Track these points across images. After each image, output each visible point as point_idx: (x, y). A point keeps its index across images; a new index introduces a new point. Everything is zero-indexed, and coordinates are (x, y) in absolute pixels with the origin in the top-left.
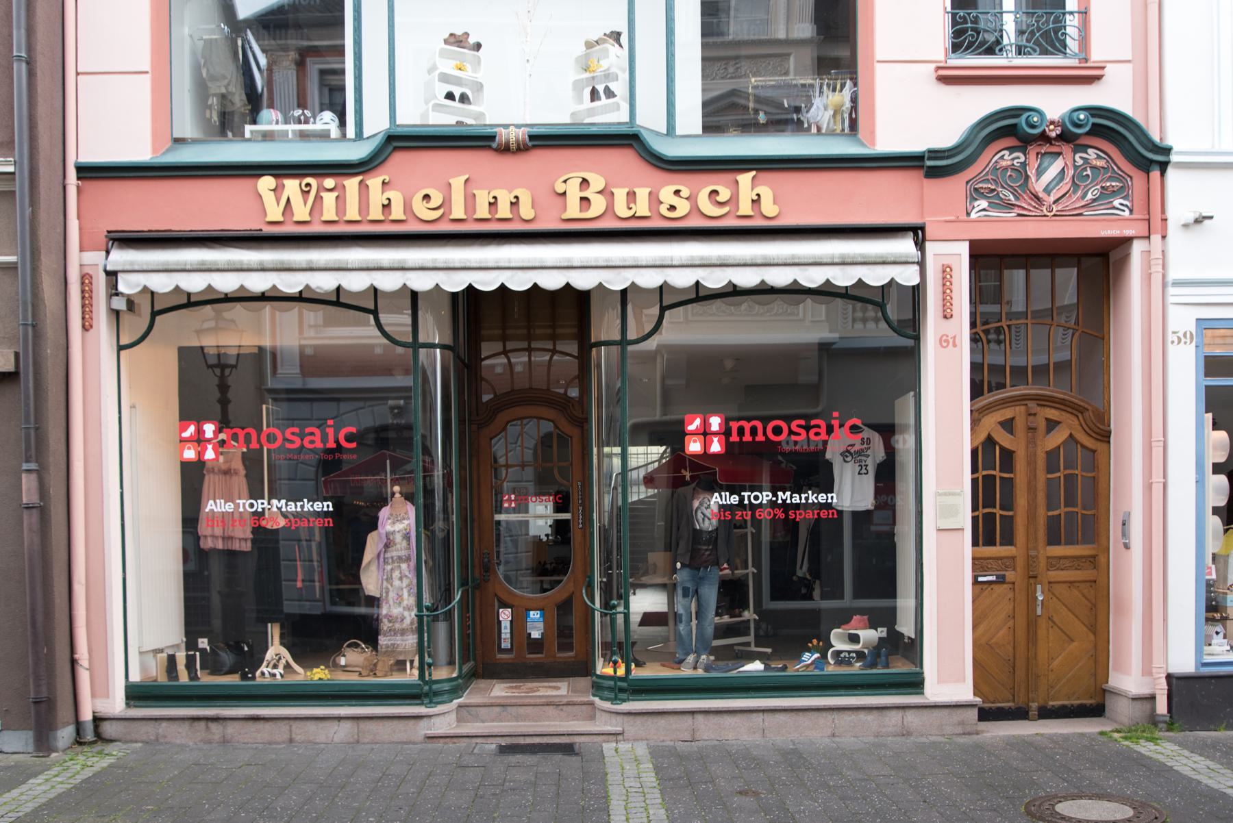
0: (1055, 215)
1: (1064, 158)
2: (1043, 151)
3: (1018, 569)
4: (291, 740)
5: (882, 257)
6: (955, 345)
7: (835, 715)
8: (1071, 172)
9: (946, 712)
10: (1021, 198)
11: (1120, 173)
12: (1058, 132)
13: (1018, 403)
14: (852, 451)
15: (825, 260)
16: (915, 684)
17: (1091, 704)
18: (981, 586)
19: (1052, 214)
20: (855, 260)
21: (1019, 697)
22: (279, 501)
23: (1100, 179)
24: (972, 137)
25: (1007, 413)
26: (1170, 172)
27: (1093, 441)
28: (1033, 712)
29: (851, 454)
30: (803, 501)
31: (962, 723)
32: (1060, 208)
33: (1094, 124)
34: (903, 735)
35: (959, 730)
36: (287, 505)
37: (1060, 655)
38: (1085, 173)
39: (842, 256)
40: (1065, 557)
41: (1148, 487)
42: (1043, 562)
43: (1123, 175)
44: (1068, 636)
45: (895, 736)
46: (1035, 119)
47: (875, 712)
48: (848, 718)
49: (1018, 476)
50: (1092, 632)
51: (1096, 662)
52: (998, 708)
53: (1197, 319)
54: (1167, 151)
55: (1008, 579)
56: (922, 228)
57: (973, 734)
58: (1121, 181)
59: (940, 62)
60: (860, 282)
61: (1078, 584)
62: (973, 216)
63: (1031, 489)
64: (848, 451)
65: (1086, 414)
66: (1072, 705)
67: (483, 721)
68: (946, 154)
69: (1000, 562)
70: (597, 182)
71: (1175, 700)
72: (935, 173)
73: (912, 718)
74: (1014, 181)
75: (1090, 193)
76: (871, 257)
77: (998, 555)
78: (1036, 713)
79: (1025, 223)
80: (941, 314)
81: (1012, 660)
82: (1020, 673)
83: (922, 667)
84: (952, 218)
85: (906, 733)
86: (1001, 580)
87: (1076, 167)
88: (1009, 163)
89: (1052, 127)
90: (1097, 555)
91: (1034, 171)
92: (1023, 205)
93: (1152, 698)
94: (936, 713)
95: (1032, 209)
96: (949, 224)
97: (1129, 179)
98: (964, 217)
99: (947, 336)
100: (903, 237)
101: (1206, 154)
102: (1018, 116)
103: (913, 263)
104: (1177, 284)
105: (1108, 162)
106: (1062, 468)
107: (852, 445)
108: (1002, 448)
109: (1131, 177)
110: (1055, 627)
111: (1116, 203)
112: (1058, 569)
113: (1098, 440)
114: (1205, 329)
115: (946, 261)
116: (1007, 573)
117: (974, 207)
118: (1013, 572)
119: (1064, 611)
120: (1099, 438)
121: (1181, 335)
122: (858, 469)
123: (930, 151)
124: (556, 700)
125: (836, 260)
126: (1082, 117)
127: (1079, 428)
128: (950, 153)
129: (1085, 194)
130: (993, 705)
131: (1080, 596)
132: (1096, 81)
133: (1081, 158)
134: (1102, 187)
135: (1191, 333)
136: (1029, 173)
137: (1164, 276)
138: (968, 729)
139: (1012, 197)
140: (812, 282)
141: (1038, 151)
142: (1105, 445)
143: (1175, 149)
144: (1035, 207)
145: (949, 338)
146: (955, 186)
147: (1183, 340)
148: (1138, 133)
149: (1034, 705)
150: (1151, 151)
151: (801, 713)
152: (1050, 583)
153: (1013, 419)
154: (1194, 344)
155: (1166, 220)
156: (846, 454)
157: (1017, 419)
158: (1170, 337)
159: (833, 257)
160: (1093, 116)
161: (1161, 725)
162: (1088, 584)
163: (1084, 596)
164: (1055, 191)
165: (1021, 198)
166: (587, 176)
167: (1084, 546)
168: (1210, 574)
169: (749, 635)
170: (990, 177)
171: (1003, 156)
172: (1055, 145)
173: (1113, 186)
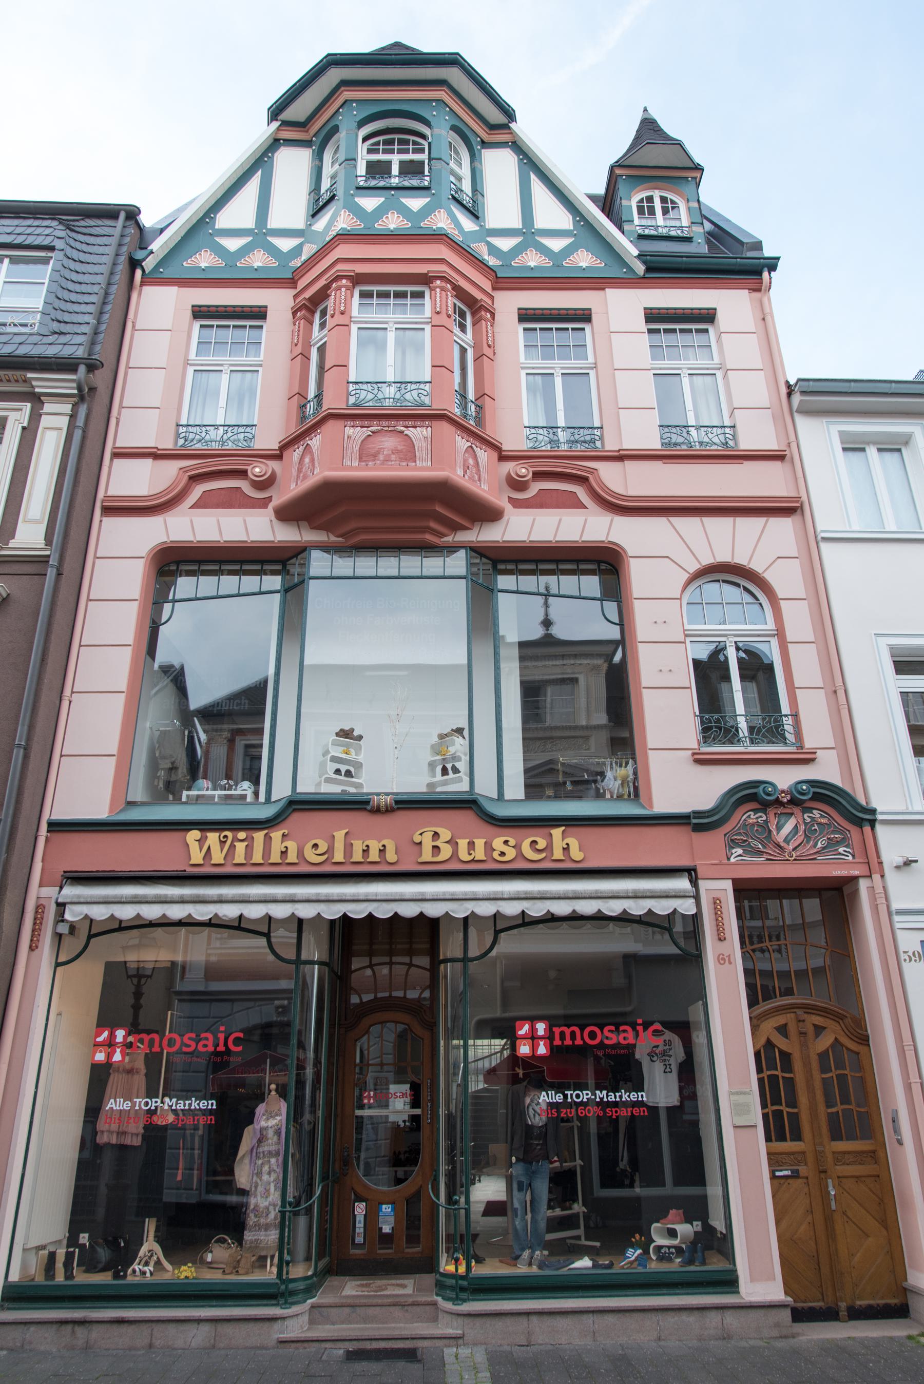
0: (795, 860)
4: (151, 1346)
5: (665, 892)
6: (730, 963)
7: (659, 1316)
9: (761, 1312)
13: (789, 1011)
16: (729, 1282)
25: (780, 1020)
26: (879, 828)
27: (856, 1045)
28: (843, 1313)
29: (656, 1054)
30: (618, 1099)
32: (798, 854)
33: (814, 793)
34: (724, 1339)
36: (607, 1096)
40: (849, 1153)
45: (717, 1339)
46: (770, 789)
47: (696, 1312)
48: (671, 1320)
52: (810, 1308)
54: (873, 811)
55: (801, 1174)
58: (841, 834)
59: (695, 749)
61: (863, 1179)
62: (732, 860)
66: (878, 1305)
67: (333, 1324)
68: (707, 814)
69: (792, 1157)
70: (445, 834)
72: (698, 828)
73: (730, 1319)
76: (657, 892)
78: (846, 1313)
80: (717, 937)
81: (816, 1256)
85: (726, 1337)
86: (795, 1175)
87: (806, 824)
89: (783, 795)
92: (770, 852)
94: (753, 1314)
98: (725, 861)
99: (723, 955)
102: (757, 787)
107: (657, 1046)
108: (781, 1051)
109: (848, 831)
111: (841, 850)
112: (844, 1164)
115: (716, 895)
116: (800, 1168)
117: (732, 854)
121: (910, 954)
123: (694, 812)
124: (402, 1300)
125: (630, 894)
126: (804, 787)
127: (843, 1033)
129: (815, 845)
134: (828, 838)
135: (918, 952)
137: (888, 907)
139: (760, 846)
140: (612, 911)
142: (865, 1048)
146: (716, 838)
147: (913, 958)
149: (843, 1305)
151: (627, 1314)
152: (839, 1177)
155: (882, 863)
158: (903, 956)
159: (627, 891)
160: (813, 787)
163: (871, 1191)
166: (438, 830)
169: (578, 1228)
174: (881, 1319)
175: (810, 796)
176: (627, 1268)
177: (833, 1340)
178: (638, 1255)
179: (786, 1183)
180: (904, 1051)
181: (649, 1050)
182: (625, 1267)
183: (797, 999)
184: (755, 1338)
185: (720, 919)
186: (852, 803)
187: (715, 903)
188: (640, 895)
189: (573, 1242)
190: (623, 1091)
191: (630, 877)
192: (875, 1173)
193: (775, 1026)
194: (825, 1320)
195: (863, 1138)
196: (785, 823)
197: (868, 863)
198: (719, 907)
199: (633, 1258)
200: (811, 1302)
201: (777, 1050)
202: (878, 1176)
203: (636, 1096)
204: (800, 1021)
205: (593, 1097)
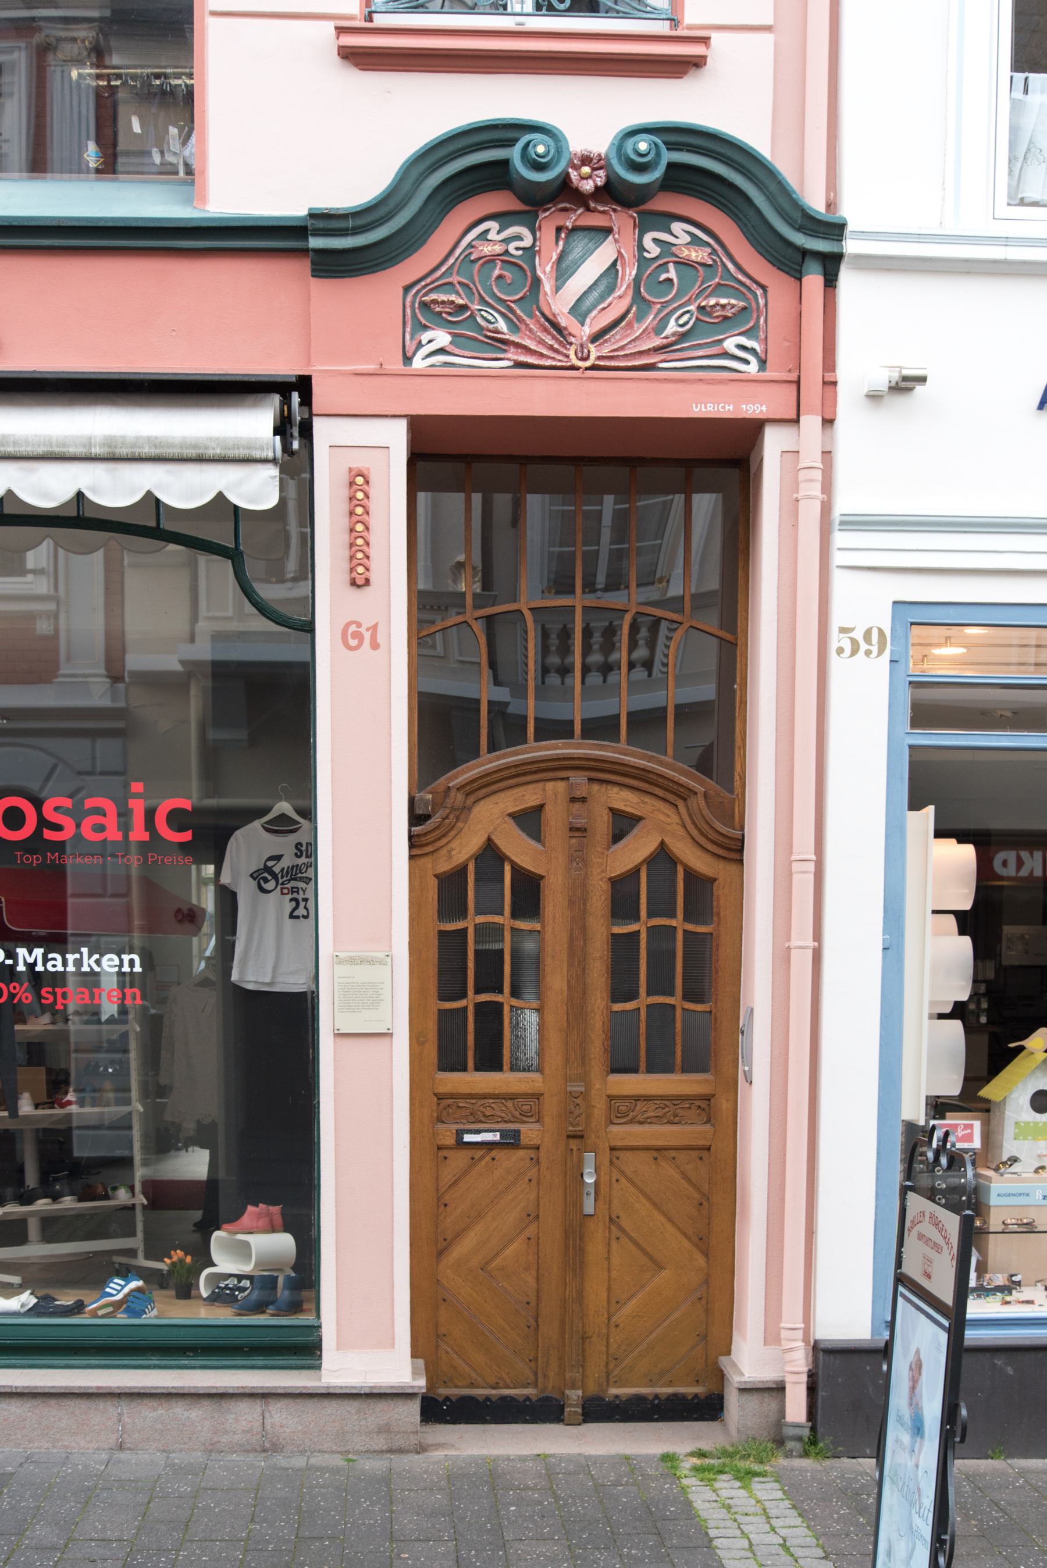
0: (593, 368)
1: (616, 241)
2: (569, 224)
3: (547, 1120)
5: (195, 446)
6: (375, 646)
7: (125, 1407)
8: (630, 273)
9: (353, 1405)
10: (523, 327)
11: (740, 277)
12: (600, 182)
13: (551, 775)
14: (277, 870)
15: (72, 450)
17: (696, 1396)
18: (470, 1153)
19: (588, 364)
20: (137, 451)
21: (545, 1376)
22: (30, 953)
23: (695, 290)
24: (407, 185)
25: (528, 797)
26: (846, 277)
27: (709, 859)
28: (573, 1409)
29: (275, 876)
30: (71, 968)
31: (385, 1429)
32: (605, 351)
33: (671, 166)
34: (265, 1451)
35: (380, 1443)
36: (45, 960)
37: (632, 1296)
38: (663, 277)
39: (110, 441)
40: (648, 1098)
41: (783, 959)
42: (599, 1106)
43: (748, 282)
44: (651, 1258)
45: (248, 1451)
46: (541, 149)
47: (206, 1403)
48: (149, 1413)
49: (549, 929)
50: (702, 1252)
51: (707, 1311)
52: (503, 1398)
53: (895, 603)
54: (836, 230)
55: (524, 1140)
56: (304, 385)
57: (408, 1451)
58: (747, 299)
59: (351, 18)
60: (151, 502)
61: (673, 1153)
62: (419, 363)
63: (577, 955)
64: (268, 869)
65: (693, 802)
66: (656, 1396)
68: (351, 223)
69: (510, 1104)
71: (822, 1394)
74: (510, 288)
75: (672, 322)
76: (173, 446)
77: (504, 1090)
78: (579, 1410)
79: (530, 381)
80: (346, 578)
81: (533, 1303)
82: (549, 1330)
83: (318, 1316)
84: (371, 367)
85: (270, 1447)
86: (511, 1141)
87: (643, 262)
88: (498, 249)
89: (586, 170)
90: (714, 1096)
91: (548, 269)
92: (528, 342)
93: (779, 1389)
94: (332, 1408)
95: (545, 352)
96: (359, 377)
97: (759, 292)
98: (398, 366)
99: (359, 625)
100: (255, 405)
101: (920, 238)
102: (510, 143)
103: (265, 461)
104: (856, 523)
105: (714, 251)
106: (643, 913)
107: (278, 858)
108: (516, 870)
109: (764, 288)
110: (624, 1240)
111: (730, 345)
112: (631, 1122)
113: (719, 856)
114: (912, 624)
115: (359, 461)
116: (523, 1128)
117: (420, 345)
118: (536, 1126)
119: (643, 1207)
120: (720, 852)
121: (858, 635)
122: (289, 906)
123: (313, 215)
125: (96, 450)
126: (643, 147)
127: (681, 832)
128: (359, 222)
129: (660, 328)
130: (494, 1392)
131: (677, 1176)
132: (693, 71)
133: (655, 240)
134: (701, 309)
135: (881, 632)
136: (539, 273)
137: (826, 508)
138: (400, 1442)
139: (502, 325)
140: (46, 496)
141: (561, 223)
142: (732, 868)
143: (850, 227)
144: (551, 348)
145: (363, 630)
147: (864, 647)
148: (773, 187)
149: (575, 1395)
150: (799, 229)
151: (53, 1402)
152: (612, 1149)
153: (541, 807)
154: (887, 656)
155: (835, 383)
156: (263, 876)
157: (547, 808)
158: (836, 640)
159: (89, 442)
160: (672, 147)
161: (790, 1445)
162: (695, 1154)
163: (686, 1177)
164: (594, 313)
165: (523, 327)
167: (686, 1077)
168: (969, 1138)
169: (133, 1234)
170: (455, 279)
171: (487, 231)
172: (594, 211)
173: (723, 306)
174: (657, 1420)
175: (657, 174)
176: (103, 1316)
177: (484, 1458)
178: (132, 1291)
179: (488, 1158)
180: (790, 875)
181: (256, 865)
182: (100, 1313)
183: (578, 746)
184: (332, 1452)
185: (359, 527)
186: (782, 200)
187: (352, 483)
188: (124, 451)
189: (124, 1260)
190: (85, 951)
191: (114, 403)
192: (701, 1143)
193: (511, 810)
194: (534, 1420)
195: (687, 1068)
196: (583, 259)
197: (798, 383)
198: (360, 495)
199: (120, 1296)
200: (508, 1387)
201: (507, 868)
202: (709, 1149)
203: (117, 962)
204: (573, 800)
205: (9, 962)
